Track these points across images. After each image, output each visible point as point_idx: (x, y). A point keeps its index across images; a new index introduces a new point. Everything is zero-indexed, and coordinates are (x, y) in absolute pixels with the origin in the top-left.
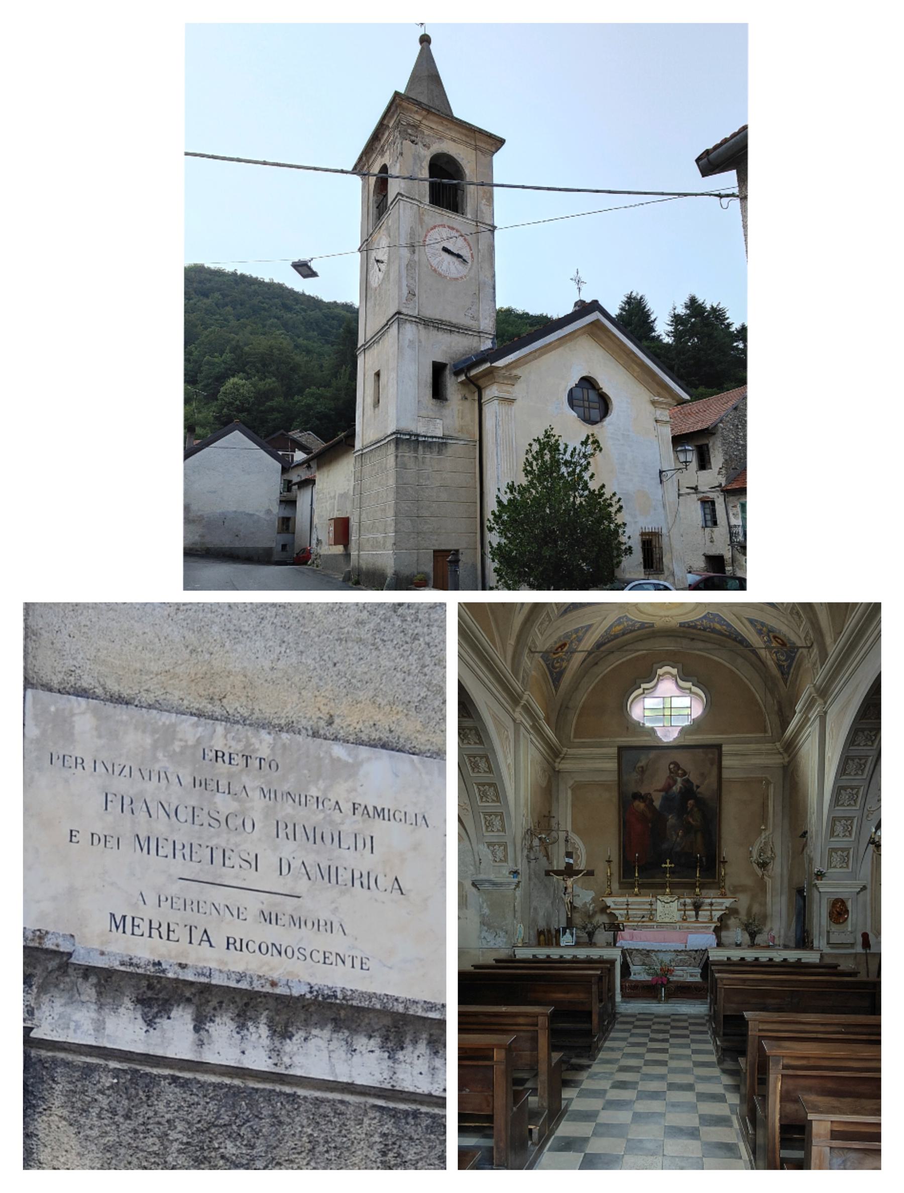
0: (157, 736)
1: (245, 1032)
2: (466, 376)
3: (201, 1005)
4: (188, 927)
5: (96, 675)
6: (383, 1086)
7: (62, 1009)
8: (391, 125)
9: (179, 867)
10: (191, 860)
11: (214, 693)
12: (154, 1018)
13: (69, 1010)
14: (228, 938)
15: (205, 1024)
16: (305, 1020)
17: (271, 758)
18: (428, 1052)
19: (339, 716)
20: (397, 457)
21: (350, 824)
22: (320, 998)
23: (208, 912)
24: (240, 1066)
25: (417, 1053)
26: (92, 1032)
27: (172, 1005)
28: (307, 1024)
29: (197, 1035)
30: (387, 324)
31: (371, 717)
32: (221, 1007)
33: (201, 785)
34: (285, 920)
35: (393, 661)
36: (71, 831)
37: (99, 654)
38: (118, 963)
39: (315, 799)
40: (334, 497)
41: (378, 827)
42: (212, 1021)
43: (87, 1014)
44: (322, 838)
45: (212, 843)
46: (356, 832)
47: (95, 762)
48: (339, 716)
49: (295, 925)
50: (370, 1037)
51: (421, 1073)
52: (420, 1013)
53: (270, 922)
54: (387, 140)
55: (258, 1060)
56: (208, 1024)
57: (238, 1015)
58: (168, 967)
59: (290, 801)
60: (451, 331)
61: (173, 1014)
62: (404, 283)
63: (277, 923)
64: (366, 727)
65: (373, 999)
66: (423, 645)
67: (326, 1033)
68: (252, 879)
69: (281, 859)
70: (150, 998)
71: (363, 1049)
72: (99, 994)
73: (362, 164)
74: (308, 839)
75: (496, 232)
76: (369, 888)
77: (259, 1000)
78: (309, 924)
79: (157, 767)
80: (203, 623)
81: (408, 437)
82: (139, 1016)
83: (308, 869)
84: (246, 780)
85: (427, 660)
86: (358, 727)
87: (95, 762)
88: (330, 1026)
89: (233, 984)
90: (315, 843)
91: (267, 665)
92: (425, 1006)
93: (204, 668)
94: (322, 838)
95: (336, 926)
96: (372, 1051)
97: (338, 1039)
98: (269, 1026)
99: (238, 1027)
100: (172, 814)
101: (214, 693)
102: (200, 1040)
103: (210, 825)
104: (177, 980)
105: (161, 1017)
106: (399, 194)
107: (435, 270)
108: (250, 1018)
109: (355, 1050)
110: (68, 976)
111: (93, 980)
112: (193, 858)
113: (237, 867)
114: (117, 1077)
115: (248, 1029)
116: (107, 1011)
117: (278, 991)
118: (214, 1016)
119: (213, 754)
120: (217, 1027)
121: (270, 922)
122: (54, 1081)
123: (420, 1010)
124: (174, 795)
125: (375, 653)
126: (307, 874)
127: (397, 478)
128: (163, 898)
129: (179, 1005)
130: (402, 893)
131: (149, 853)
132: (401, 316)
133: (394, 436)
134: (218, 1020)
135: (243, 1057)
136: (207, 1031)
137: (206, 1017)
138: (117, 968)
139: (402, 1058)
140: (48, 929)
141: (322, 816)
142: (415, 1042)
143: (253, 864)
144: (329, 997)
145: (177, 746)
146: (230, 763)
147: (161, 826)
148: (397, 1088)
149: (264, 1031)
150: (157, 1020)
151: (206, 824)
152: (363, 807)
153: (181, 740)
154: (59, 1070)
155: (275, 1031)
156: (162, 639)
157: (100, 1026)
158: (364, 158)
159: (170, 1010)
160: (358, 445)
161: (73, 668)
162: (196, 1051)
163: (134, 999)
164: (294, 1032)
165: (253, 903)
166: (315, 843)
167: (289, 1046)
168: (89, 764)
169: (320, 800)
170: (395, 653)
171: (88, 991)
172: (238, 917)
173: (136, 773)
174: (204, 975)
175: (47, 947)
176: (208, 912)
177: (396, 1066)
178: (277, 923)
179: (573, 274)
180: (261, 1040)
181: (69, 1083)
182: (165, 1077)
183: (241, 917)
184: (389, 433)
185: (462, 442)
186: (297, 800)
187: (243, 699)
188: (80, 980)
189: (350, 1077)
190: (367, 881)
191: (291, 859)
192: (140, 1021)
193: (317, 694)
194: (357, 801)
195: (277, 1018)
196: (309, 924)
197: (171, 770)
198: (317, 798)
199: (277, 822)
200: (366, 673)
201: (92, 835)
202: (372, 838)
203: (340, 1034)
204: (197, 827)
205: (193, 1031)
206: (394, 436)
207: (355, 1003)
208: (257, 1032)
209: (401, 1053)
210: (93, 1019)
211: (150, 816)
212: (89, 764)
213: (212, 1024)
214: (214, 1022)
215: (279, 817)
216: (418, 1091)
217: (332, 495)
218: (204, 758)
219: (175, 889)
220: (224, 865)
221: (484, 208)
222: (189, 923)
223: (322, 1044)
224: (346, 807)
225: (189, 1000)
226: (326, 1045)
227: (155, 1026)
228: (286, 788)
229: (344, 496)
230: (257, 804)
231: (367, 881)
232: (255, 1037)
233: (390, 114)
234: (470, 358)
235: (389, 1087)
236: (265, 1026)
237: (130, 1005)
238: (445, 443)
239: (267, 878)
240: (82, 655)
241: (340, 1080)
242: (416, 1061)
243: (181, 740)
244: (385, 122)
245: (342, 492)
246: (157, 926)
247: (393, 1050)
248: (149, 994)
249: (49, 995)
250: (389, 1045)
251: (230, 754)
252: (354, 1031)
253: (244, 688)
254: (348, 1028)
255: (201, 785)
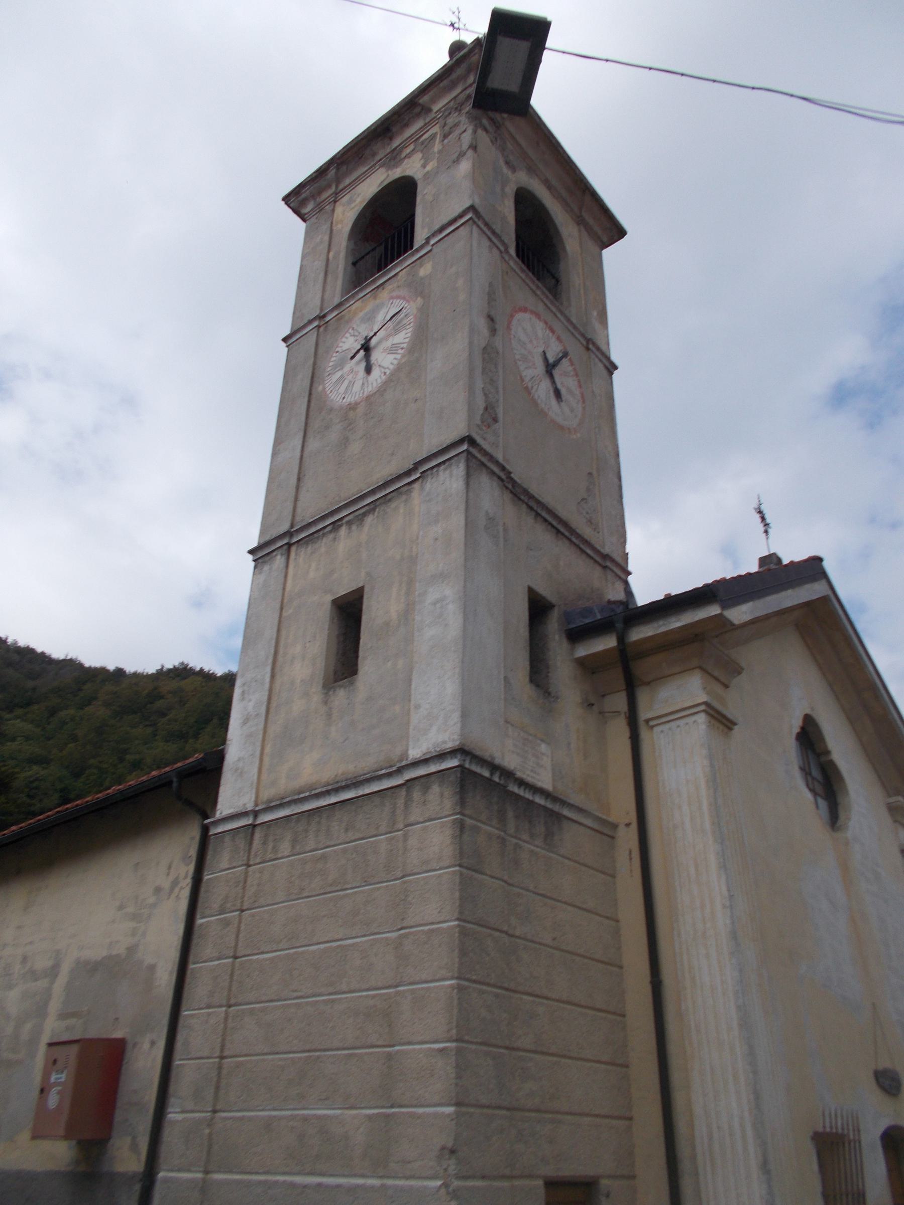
2: (621, 640)
8: (435, 108)
20: (461, 827)
30: (408, 473)
40: (53, 972)
54: (415, 139)
60: (558, 531)
62: (479, 384)
73: (322, 183)
75: (616, 375)
81: (486, 774)
106: (472, 208)
107: (528, 390)
127: (461, 898)
132: (474, 451)
133: (453, 763)
158: (332, 173)
160: (233, 795)
179: (755, 504)
184: (415, 753)
185: (588, 822)
206: (453, 763)
217: (42, 963)
221: (597, 326)
229: (110, 969)
233: (445, 83)
234: (587, 611)
238: (559, 817)
244: (424, 99)
245: (96, 954)
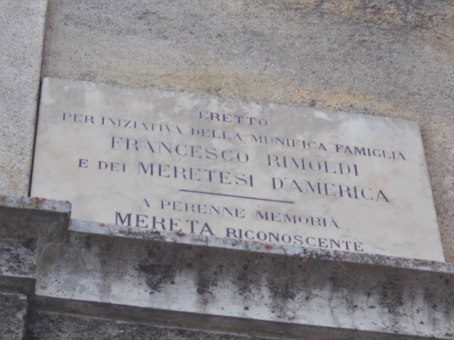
0: (158, 104)
1: (248, 293)
3: (202, 270)
4: (190, 222)
5: (108, 76)
6: (386, 331)
7: (67, 277)
9: (180, 183)
10: (191, 178)
11: (210, 87)
12: (158, 283)
13: (75, 277)
14: (228, 230)
15: (208, 288)
16: (304, 281)
17: (260, 118)
18: (426, 306)
19: (320, 101)
21: (334, 159)
22: (314, 257)
23: (208, 212)
24: (244, 317)
25: (416, 307)
26: (98, 293)
27: (174, 271)
28: (306, 283)
29: (201, 296)
31: (348, 102)
32: (221, 271)
33: (198, 133)
34: (282, 217)
35: (363, 71)
36: (81, 160)
37: (111, 65)
38: (117, 231)
39: (302, 143)
41: (360, 160)
42: (215, 285)
43: (93, 281)
44: (310, 166)
45: (211, 168)
46: (340, 162)
47: (103, 119)
48: (320, 101)
49: (290, 221)
50: (369, 295)
51: (422, 323)
52: (411, 266)
53: (267, 219)
55: (261, 312)
56: (211, 288)
57: (239, 279)
58: (166, 235)
59: (279, 143)
61: (176, 279)
63: (273, 219)
64: (344, 107)
65: (365, 258)
66: (387, 63)
67: (326, 293)
68: (247, 190)
69: (274, 179)
70: (153, 266)
71: (364, 305)
72: (104, 263)
74: (297, 166)
76: (356, 197)
77: (257, 262)
78: (304, 220)
79: (159, 122)
80: (199, 49)
82: (143, 281)
83: (299, 185)
84: (238, 130)
85: (392, 71)
86: (337, 107)
87: (103, 119)
88: (329, 286)
89: (229, 246)
90: (304, 168)
91: (255, 72)
92: (416, 262)
93: (202, 73)
94: (310, 166)
95: (328, 222)
96: (373, 307)
97: (338, 297)
98: (270, 288)
99: (241, 289)
100: (174, 151)
101: (210, 87)
102: (204, 299)
103: (207, 157)
104: (175, 244)
105: (165, 282)
108: (251, 281)
109: (356, 306)
110: (71, 245)
111: (95, 249)
112: (193, 178)
113: (234, 184)
114: (124, 329)
115: (250, 291)
116: (112, 278)
117: (273, 251)
118: (216, 280)
119: (209, 115)
120: (220, 290)
121: (267, 219)
122: (60, 331)
123: (412, 265)
124: (174, 139)
125: (347, 67)
126: (299, 188)
128: (165, 203)
129: (181, 271)
130: (387, 201)
131: (152, 174)
134: (220, 283)
135: (246, 311)
136: (211, 293)
137: (208, 281)
138: (116, 235)
139: (401, 311)
140: (45, 197)
141: (308, 152)
142: (412, 298)
143: (249, 182)
144: (322, 256)
145: (176, 110)
146: (224, 120)
147: (162, 157)
148: (400, 333)
149: (266, 292)
150: (160, 285)
151: (204, 156)
152: (345, 147)
153: (180, 107)
154: (65, 323)
155: (277, 292)
156: (165, 57)
157: (105, 289)
159: (174, 276)
161: (88, 72)
162: (200, 307)
163: (137, 267)
164: (295, 293)
165: (250, 207)
166: (304, 168)
167: (291, 304)
168: (97, 120)
169: (306, 143)
170: (363, 67)
171: (92, 259)
172: (237, 215)
173: (139, 125)
174: (201, 240)
175: (44, 208)
176: (208, 212)
177: (398, 318)
178: (273, 219)
180: (264, 300)
181: (75, 332)
182: (172, 331)
183: (239, 215)
186: (285, 142)
187: (236, 91)
188: (83, 250)
189: (353, 325)
190: (354, 193)
191: (283, 179)
192: (145, 286)
193: (300, 88)
194: (340, 143)
195: (277, 280)
196: (304, 220)
197: (171, 124)
198: (304, 142)
199: (269, 157)
200: (340, 77)
201: (100, 163)
202: (355, 166)
203: (340, 293)
204: (196, 159)
205: (196, 293)
207: (347, 260)
208: (259, 294)
209: (400, 308)
210: (99, 284)
211: (153, 151)
212: (97, 120)
213: (215, 288)
214: (216, 285)
215: (270, 153)
216: (421, 335)
218: (201, 117)
219: (177, 197)
220: (222, 182)
222: (191, 219)
223: (324, 302)
224: (331, 148)
225: (190, 266)
226: (328, 303)
227: (159, 289)
228: (275, 135)
230: (249, 146)
231: (354, 193)
232: (257, 298)
235: (392, 332)
236: (267, 289)
237: (134, 272)
239: (262, 188)
240: (96, 65)
241: (344, 327)
242: (416, 314)
243: (180, 107)
246: (161, 221)
247: (392, 306)
248: (151, 261)
249: (56, 265)
250: (388, 301)
251: (224, 116)
252: (353, 290)
253: (237, 85)
254: (346, 287)
255: (198, 133)
